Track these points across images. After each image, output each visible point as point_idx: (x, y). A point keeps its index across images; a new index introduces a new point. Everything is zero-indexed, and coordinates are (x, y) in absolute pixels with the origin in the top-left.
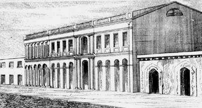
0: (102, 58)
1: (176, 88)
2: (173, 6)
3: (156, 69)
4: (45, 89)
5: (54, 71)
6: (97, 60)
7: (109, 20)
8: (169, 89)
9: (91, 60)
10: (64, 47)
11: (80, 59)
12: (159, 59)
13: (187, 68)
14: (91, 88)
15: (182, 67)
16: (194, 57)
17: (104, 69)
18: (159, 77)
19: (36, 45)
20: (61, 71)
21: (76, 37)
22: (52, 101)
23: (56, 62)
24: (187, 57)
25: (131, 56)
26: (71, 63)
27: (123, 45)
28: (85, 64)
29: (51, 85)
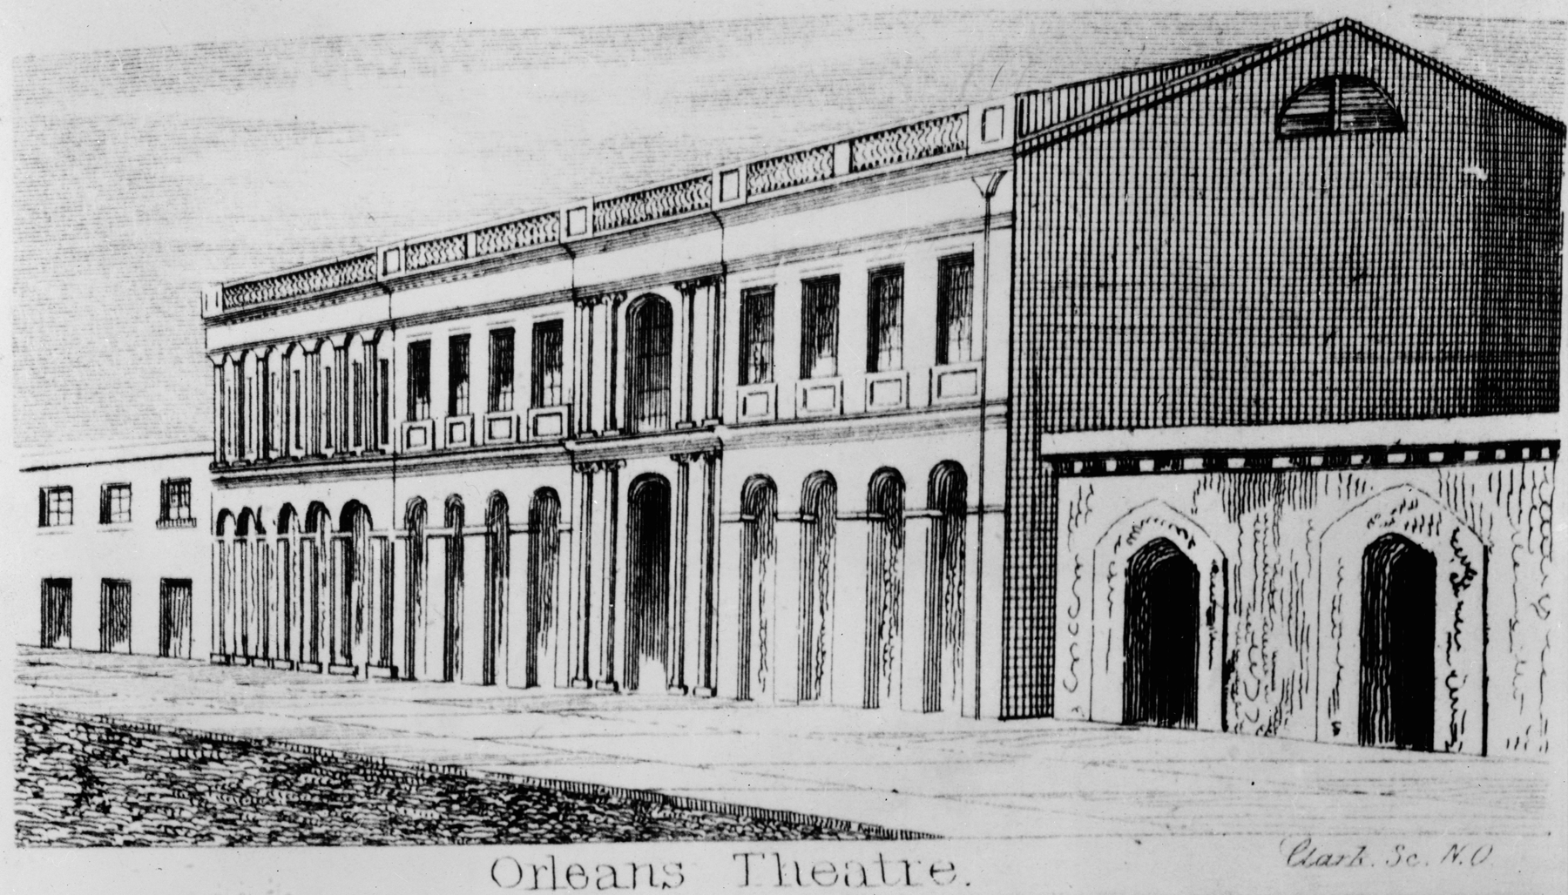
0: (839, 447)
1: (1325, 694)
2: (1332, 60)
3: (1181, 543)
4: (345, 688)
5: (417, 555)
6: (736, 470)
7: (842, 165)
8: (1275, 697)
9: (697, 468)
10: (502, 372)
11: (613, 467)
12: (1208, 469)
13: (1418, 538)
14: (690, 680)
15: (1377, 532)
16: (1471, 455)
17: (788, 535)
18: (1204, 604)
19: (297, 359)
20: (475, 551)
21: (583, 298)
22: (399, 779)
23: (435, 487)
24: (1418, 456)
25: (996, 436)
26: (546, 494)
27: (942, 357)
28: (651, 499)
29: (399, 659)
